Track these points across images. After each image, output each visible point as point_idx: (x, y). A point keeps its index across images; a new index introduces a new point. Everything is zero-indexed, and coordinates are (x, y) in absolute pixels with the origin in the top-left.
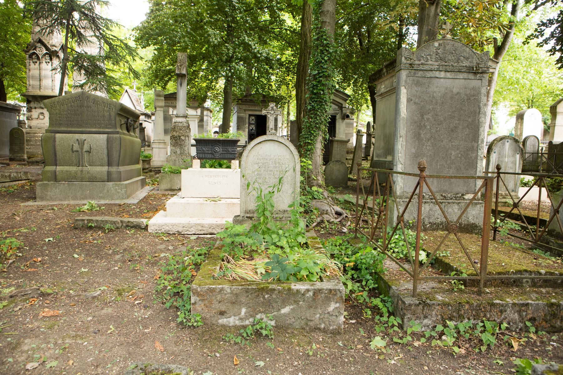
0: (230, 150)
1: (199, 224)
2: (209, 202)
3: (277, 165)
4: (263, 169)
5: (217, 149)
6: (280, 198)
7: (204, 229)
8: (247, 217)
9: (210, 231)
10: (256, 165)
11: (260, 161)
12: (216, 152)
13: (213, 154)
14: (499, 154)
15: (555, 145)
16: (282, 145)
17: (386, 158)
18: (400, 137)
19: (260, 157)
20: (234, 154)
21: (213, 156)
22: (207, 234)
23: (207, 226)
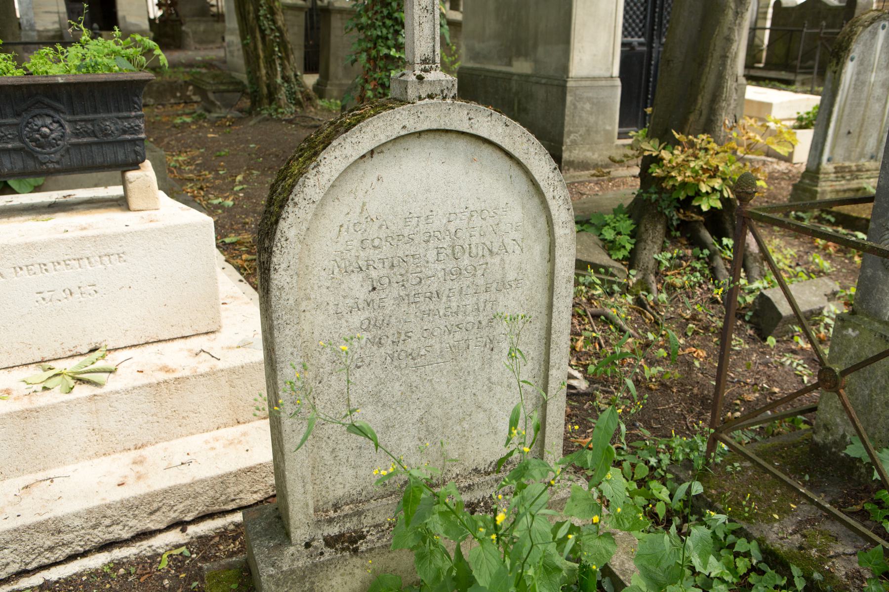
0: (110, 126)
1: (38, 527)
2: (56, 396)
3: (466, 261)
4: (396, 291)
5: (47, 127)
6: (480, 417)
7: (67, 537)
8: (330, 542)
9: (101, 535)
10: (357, 278)
11: (374, 255)
12: (44, 142)
13: (31, 154)
14: (861, 63)
15: (787, 9)
16: (487, 150)
17: (510, 64)
18: (852, 60)
19: (373, 231)
20: (133, 142)
21: (31, 164)
22: (84, 554)
23: (77, 522)
